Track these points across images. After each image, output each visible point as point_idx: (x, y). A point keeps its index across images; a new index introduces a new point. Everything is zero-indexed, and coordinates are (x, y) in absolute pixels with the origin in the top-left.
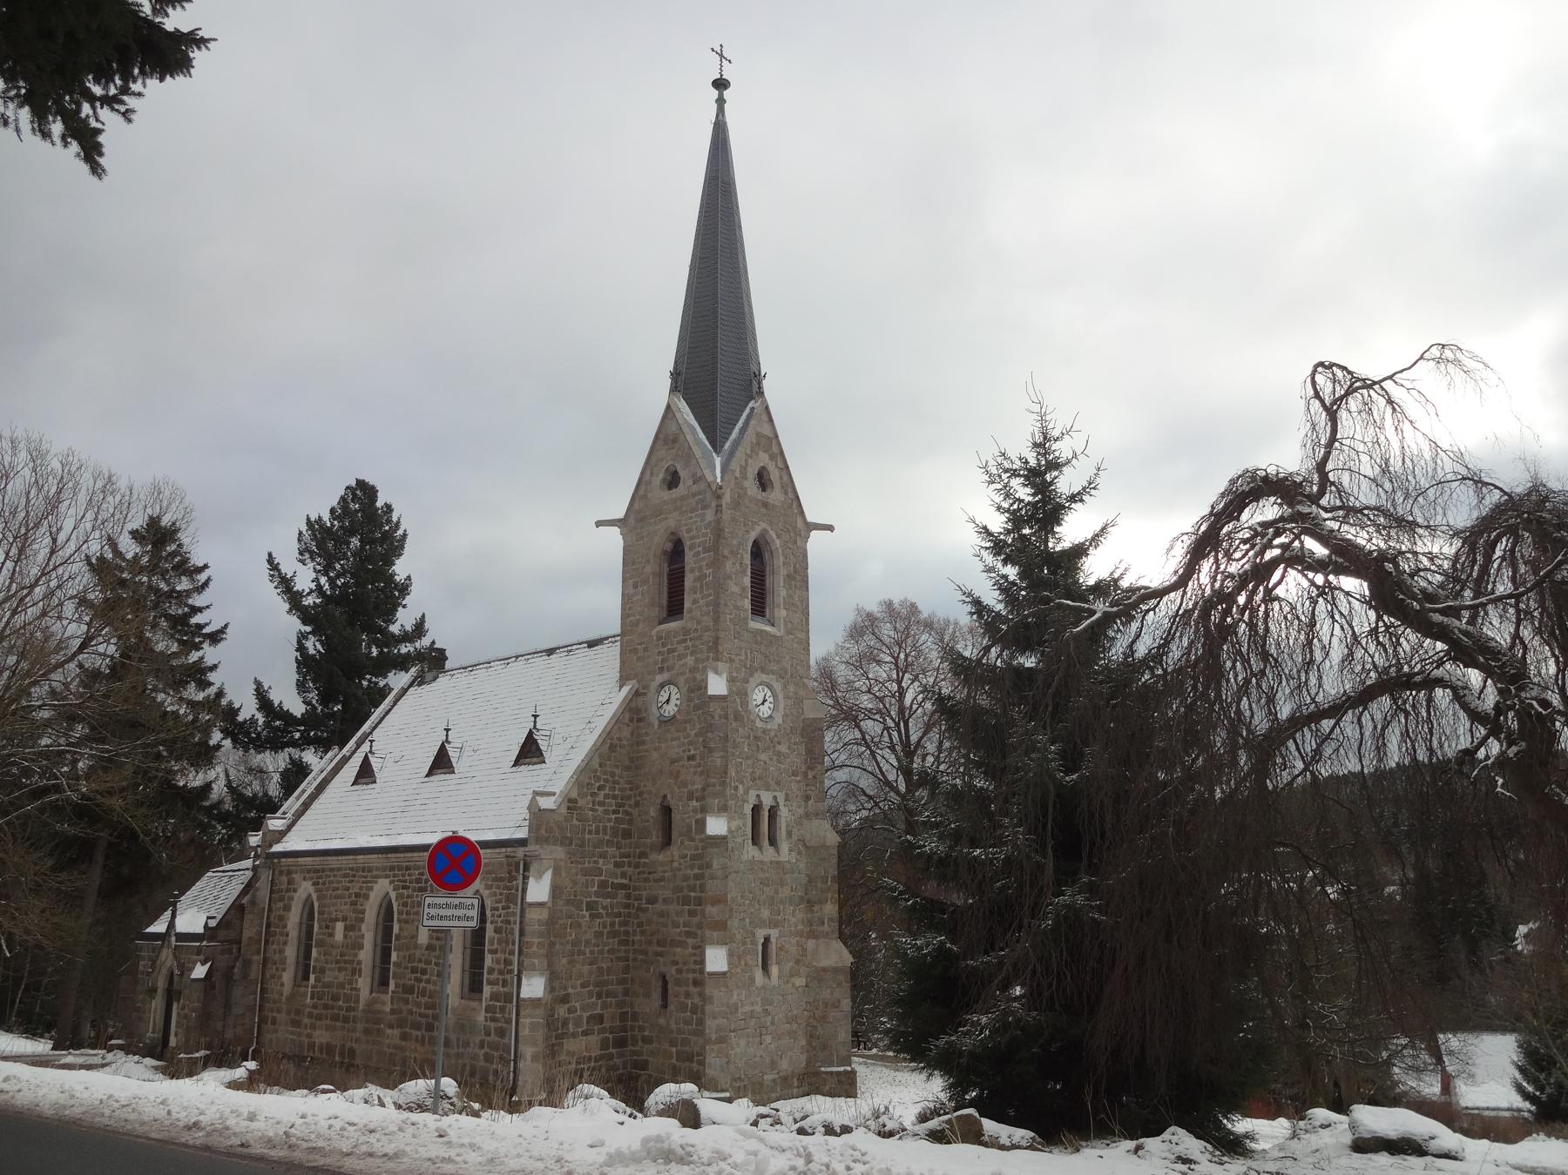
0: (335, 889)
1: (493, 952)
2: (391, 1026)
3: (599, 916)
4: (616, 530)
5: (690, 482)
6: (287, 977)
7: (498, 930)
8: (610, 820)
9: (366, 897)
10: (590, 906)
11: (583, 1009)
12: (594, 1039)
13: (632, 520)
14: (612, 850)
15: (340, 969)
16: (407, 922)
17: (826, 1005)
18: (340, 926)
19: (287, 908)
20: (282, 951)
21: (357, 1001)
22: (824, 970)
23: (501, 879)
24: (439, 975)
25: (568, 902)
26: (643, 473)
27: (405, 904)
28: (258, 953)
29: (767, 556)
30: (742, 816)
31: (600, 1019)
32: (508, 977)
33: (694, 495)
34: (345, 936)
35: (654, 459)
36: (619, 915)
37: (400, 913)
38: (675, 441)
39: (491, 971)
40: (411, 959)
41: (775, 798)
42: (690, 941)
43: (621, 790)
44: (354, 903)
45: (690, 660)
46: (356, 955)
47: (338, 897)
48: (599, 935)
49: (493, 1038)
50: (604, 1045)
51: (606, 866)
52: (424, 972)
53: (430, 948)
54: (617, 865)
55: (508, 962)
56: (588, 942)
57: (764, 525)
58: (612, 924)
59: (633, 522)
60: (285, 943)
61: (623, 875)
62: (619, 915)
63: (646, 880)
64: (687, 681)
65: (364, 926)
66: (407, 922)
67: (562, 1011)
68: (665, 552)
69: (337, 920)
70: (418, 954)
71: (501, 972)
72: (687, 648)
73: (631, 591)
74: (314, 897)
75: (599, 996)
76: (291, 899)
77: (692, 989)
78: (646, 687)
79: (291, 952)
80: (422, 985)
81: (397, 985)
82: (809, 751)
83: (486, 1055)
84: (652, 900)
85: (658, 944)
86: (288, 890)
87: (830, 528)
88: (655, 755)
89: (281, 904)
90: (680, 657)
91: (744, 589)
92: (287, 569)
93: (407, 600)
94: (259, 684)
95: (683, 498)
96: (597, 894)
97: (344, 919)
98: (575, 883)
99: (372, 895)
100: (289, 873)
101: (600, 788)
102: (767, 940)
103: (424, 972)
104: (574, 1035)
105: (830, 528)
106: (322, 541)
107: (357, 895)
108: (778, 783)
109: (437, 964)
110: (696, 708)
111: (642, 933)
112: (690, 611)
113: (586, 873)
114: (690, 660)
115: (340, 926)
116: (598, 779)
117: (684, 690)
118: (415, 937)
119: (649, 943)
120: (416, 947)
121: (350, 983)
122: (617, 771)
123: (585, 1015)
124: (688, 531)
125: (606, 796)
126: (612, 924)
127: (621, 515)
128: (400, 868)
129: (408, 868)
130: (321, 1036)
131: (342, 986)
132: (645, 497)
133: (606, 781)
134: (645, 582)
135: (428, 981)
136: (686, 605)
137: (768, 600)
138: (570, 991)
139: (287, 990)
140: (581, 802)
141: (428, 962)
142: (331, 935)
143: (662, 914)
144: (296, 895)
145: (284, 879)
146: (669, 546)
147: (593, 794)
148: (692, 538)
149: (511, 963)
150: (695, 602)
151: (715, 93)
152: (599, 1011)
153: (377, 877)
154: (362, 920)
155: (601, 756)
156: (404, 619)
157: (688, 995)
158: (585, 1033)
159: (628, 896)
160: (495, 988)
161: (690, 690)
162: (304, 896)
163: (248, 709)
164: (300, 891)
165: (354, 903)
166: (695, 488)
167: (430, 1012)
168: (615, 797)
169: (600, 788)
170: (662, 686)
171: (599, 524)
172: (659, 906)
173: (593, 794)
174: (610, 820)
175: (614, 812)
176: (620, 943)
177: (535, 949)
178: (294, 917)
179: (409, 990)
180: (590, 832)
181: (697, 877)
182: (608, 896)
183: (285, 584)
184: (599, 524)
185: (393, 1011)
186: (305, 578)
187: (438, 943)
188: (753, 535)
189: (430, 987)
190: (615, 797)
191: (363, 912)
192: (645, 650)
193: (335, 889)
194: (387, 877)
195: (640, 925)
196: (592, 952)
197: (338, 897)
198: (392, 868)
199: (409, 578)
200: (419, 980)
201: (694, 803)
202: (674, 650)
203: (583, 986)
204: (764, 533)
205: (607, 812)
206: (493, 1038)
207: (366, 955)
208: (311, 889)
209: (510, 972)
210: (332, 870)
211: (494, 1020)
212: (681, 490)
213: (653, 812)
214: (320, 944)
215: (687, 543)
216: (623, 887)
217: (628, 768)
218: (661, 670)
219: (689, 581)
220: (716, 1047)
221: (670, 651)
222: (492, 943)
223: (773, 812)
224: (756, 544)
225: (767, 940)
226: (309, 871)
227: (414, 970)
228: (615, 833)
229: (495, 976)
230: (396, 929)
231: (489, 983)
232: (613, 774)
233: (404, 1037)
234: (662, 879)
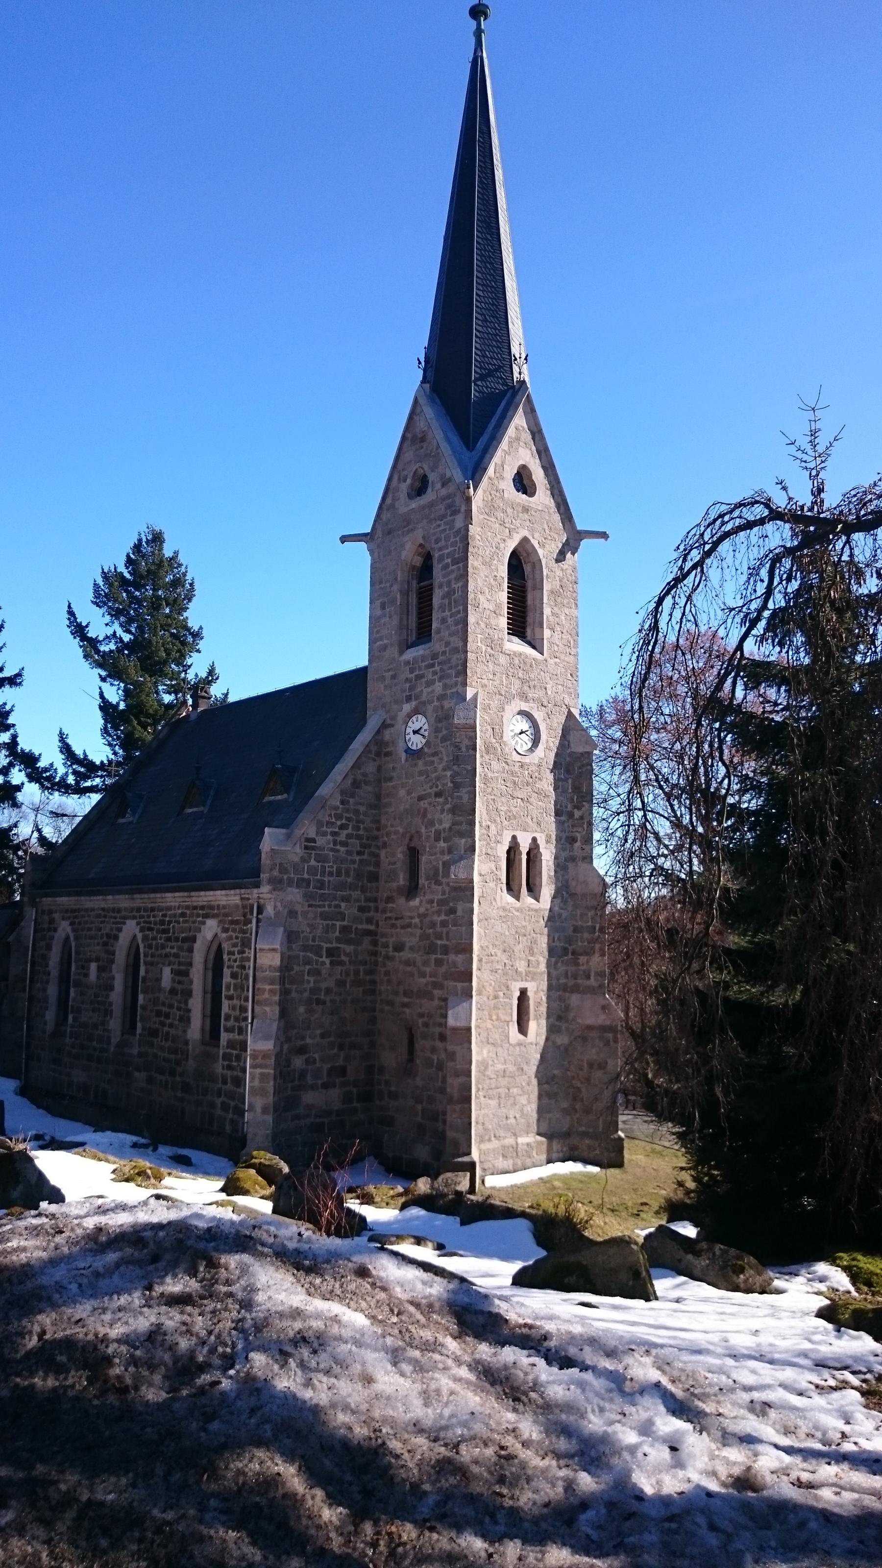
0: (90, 929)
1: (230, 998)
2: (138, 1069)
3: (341, 963)
4: (363, 545)
5: (439, 486)
6: (50, 1015)
7: (234, 976)
8: (353, 862)
9: (116, 938)
10: (330, 953)
11: (323, 1060)
12: (335, 1094)
13: (379, 533)
14: (357, 894)
15: (94, 1010)
16: (152, 964)
17: (591, 1065)
18: (93, 966)
19: (49, 947)
20: (45, 990)
21: (109, 1043)
22: (590, 1028)
23: (237, 922)
24: (181, 1019)
25: (305, 948)
26: (390, 480)
27: (150, 947)
28: (24, 991)
29: (527, 569)
30: (496, 859)
31: (343, 1071)
32: (243, 1024)
33: (444, 499)
34: (98, 977)
35: (400, 466)
36: (365, 963)
37: (146, 955)
38: (423, 439)
39: (228, 1018)
40: (156, 1002)
41: (534, 840)
42: (437, 992)
43: (366, 829)
44: (105, 944)
45: (438, 687)
46: (107, 996)
47: (91, 938)
48: (341, 983)
49: (229, 1086)
50: (347, 1098)
51: (349, 910)
52: (167, 1016)
53: (173, 991)
54: (361, 909)
55: (244, 1009)
56: (328, 991)
57: (524, 533)
58: (357, 973)
59: (380, 537)
60: (48, 982)
61: (369, 921)
62: (365, 963)
63: (393, 926)
64: (436, 710)
65: (114, 967)
66: (152, 964)
67: (298, 1062)
68: (413, 568)
69: (91, 960)
70: (162, 997)
71: (237, 1019)
72: (435, 673)
73: (379, 612)
74: (140, 936)
75: (341, 1047)
76: (52, 938)
77: (439, 1044)
78: (394, 718)
79: (52, 991)
80: (166, 1029)
81: (144, 1029)
82: (577, 789)
83: (223, 1103)
84: (399, 948)
85: (405, 994)
86: (49, 930)
87: (604, 535)
88: (402, 793)
89: (43, 943)
90: (430, 683)
91: (499, 606)
92: (82, 619)
93: (201, 645)
94: (61, 734)
95: (432, 504)
96: (338, 940)
97: (97, 960)
98: (312, 927)
99: (122, 936)
100: (50, 912)
101: (342, 827)
102: (523, 993)
103: (167, 1016)
104: (313, 1088)
105: (604, 535)
106: (115, 592)
107: (108, 936)
108: (539, 824)
109: (179, 1009)
110: (444, 739)
111: (389, 982)
112: (438, 631)
113: (324, 916)
114: (438, 687)
115: (93, 966)
116: (339, 817)
117: (432, 720)
118: (159, 980)
119: (396, 993)
120: (160, 990)
121: (103, 1024)
122: (362, 809)
123: (326, 1067)
124: (437, 541)
125: (349, 836)
126: (357, 973)
127: (368, 529)
128: (146, 909)
129: (153, 909)
130: (79, 1076)
131: (95, 1026)
132: (392, 507)
133: (349, 819)
134: (393, 602)
135: (171, 1026)
136: (434, 625)
137: (530, 619)
138: (308, 1041)
139: (50, 1027)
140: (321, 841)
141: (171, 1006)
142: (86, 975)
143: (408, 963)
144: (57, 935)
145: (46, 918)
146: (418, 561)
147: (334, 834)
148: (440, 549)
149: (246, 1011)
150: (444, 621)
151: (474, 23)
152: (340, 1062)
153: (125, 918)
154: (112, 961)
155: (343, 792)
156: (197, 666)
157: (434, 1050)
158: (325, 1086)
159: (375, 943)
160: (231, 1036)
161: (439, 720)
162: (63, 935)
163: (51, 757)
164: (60, 930)
165: (105, 944)
166: (444, 492)
167: (172, 1057)
168: (359, 837)
169: (342, 827)
170: (410, 716)
171: (344, 539)
172: (406, 955)
173: (334, 834)
174: (353, 862)
175: (359, 853)
176: (365, 992)
177: (266, 996)
178: (54, 958)
179: (154, 1033)
180: (331, 874)
181: (444, 924)
182: (349, 942)
183: (79, 631)
184: (344, 539)
185: (140, 1055)
186: (99, 624)
187: (179, 987)
188: (512, 545)
189: (173, 1031)
190: (359, 837)
191: (113, 953)
192: (394, 677)
193: (90, 929)
194: (134, 918)
195: (387, 973)
196: (332, 1001)
197: (91, 938)
198: (138, 910)
199: (201, 628)
200: (163, 1024)
201: (442, 844)
202: (421, 676)
203: (323, 1036)
204: (525, 541)
205: (349, 853)
206: (229, 1086)
207: (117, 996)
208: (69, 929)
209: (246, 1019)
210: (87, 910)
211: (230, 1067)
212: (430, 495)
213: (400, 855)
214: (77, 984)
215: (436, 555)
216: (369, 933)
217: (371, 806)
218: (409, 699)
219: (437, 600)
220: (458, 1107)
221: (419, 677)
222: (228, 988)
223: (533, 854)
224: (514, 555)
225: (523, 993)
226: (67, 911)
227: (159, 1014)
228: (358, 876)
229: (231, 1023)
230: (142, 972)
231: (227, 1030)
232: (357, 812)
233: (150, 1080)
234: (409, 926)
